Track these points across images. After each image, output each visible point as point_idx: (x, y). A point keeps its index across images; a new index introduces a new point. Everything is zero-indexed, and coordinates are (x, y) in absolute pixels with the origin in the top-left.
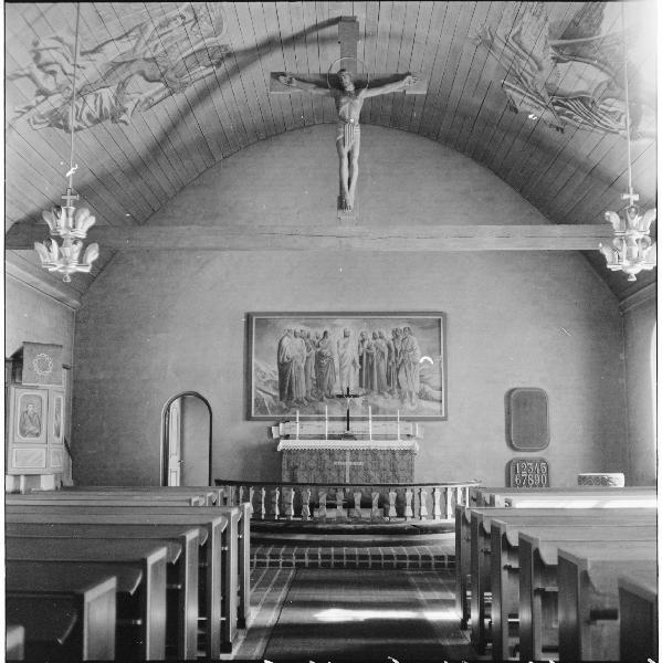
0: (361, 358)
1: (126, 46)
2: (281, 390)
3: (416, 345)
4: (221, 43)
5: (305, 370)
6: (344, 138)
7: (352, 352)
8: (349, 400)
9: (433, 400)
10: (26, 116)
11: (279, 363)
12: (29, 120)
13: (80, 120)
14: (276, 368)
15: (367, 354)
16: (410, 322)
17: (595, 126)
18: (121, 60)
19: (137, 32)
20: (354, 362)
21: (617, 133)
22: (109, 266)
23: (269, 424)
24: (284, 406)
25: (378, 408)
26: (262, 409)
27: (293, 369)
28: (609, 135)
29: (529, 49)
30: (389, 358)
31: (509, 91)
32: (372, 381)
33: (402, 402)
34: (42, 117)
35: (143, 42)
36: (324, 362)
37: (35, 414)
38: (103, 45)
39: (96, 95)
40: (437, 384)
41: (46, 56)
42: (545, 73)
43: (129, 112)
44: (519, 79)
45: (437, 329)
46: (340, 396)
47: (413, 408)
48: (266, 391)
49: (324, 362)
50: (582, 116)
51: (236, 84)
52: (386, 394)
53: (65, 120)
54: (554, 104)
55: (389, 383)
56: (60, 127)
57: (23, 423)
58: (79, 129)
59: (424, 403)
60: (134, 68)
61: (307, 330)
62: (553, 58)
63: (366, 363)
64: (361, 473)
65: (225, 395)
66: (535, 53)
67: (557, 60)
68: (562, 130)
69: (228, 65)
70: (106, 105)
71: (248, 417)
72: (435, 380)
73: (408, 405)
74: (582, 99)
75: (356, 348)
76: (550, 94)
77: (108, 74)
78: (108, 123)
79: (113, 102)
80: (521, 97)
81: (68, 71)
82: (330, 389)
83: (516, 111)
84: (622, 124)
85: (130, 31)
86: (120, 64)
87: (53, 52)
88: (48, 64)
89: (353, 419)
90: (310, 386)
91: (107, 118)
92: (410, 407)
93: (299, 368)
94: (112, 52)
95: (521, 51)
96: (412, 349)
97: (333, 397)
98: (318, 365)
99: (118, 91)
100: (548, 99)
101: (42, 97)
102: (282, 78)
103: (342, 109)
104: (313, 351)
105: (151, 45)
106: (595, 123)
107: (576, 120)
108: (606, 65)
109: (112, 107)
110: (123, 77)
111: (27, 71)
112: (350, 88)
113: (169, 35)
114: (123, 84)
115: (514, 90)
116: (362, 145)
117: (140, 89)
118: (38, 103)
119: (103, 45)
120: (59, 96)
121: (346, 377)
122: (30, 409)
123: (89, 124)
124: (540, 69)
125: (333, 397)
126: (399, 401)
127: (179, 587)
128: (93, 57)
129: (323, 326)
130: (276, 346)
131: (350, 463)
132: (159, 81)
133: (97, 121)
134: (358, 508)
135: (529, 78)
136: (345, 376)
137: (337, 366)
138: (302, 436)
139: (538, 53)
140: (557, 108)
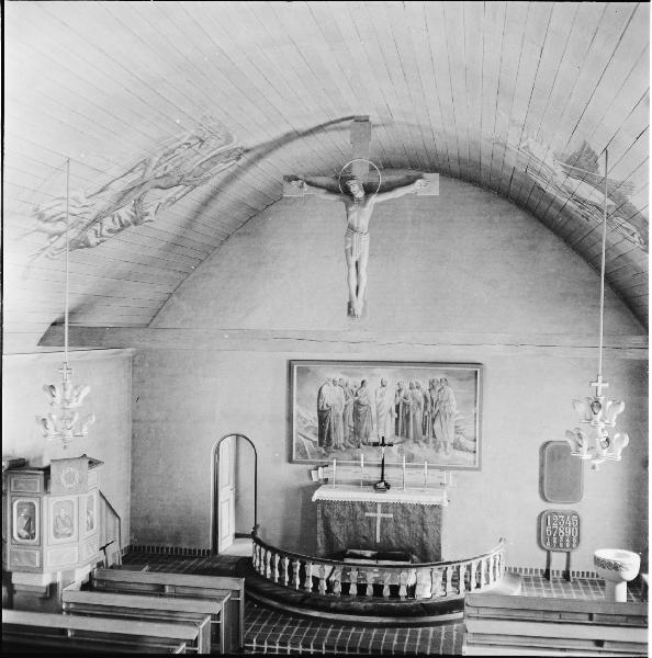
0: (397, 407)
2: (321, 436)
3: (452, 396)
5: (344, 417)
6: (352, 248)
7: (389, 402)
8: (383, 449)
9: (467, 450)
11: (319, 410)
15: (404, 404)
16: (447, 373)
22: (161, 312)
23: (310, 467)
25: (413, 455)
26: (304, 454)
27: (332, 416)
30: (425, 408)
33: (437, 451)
36: (362, 410)
37: (67, 517)
40: (471, 435)
41: (49, 214)
45: (474, 381)
46: (376, 444)
47: (448, 457)
48: (307, 435)
49: (362, 410)
51: (253, 171)
52: (422, 443)
55: (424, 433)
57: (56, 526)
59: (458, 454)
60: (146, 187)
61: (345, 378)
63: (402, 413)
64: (391, 526)
65: (269, 441)
69: (248, 156)
71: (290, 460)
72: (469, 431)
73: (442, 454)
82: (367, 436)
89: (388, 465)
90: (348, 433)
91: (129, 225)
92: (444, 457)
93: (338, 416)
97: (369, 444)
98: (356, 414)
103: (350, 218)
104: (351, 400)
110: (137, 196)
112: (360, 194)
116: (371, 255)
121: (382, 426)
122: (62, 513)
125: (369, 444)
126: (433, 451)
129: (361, 375)
131: (382, 515)
136: (383, 425)
137: (374, 414)
138: (341, 487)
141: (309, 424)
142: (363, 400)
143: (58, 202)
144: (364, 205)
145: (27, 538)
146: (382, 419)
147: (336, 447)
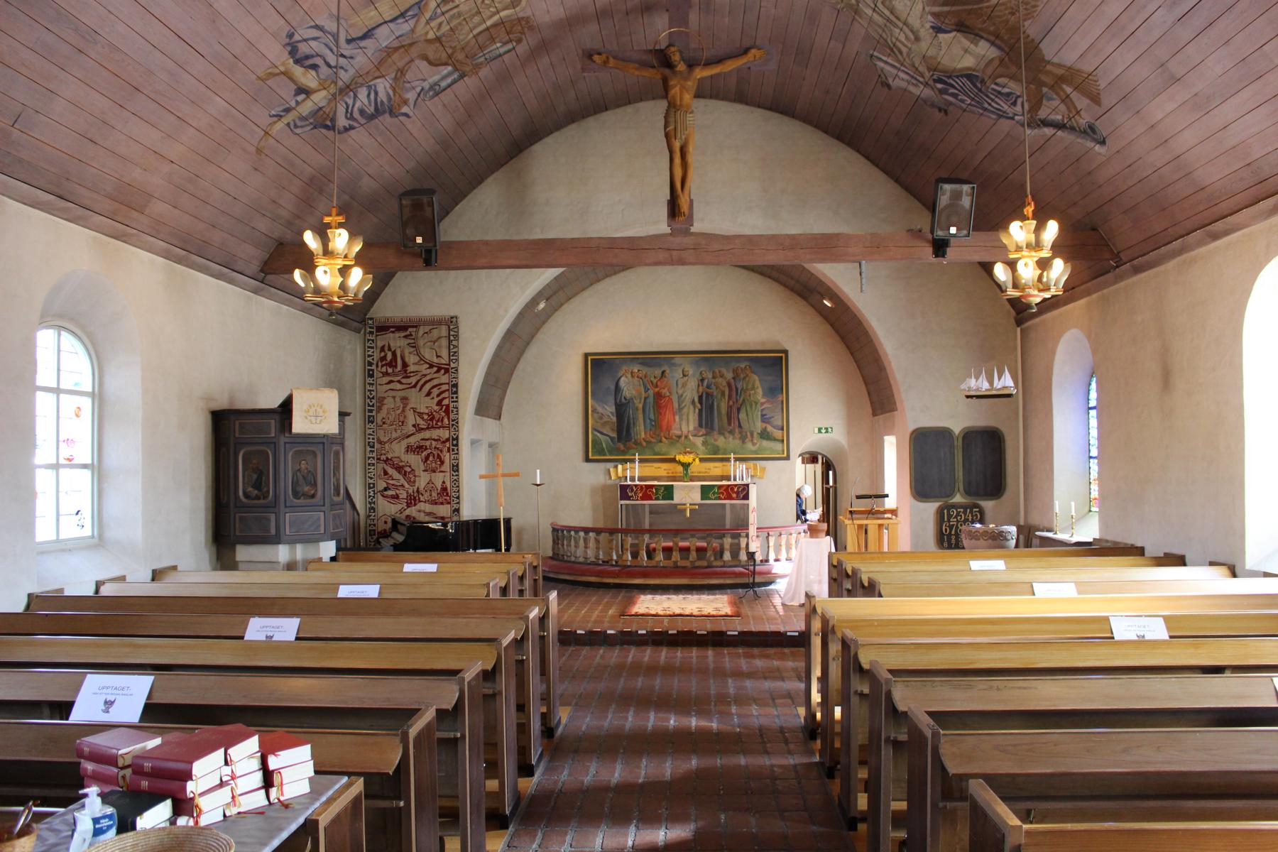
0: (700, 398)
1: (404, 27)
2: (619, 431)
4: (521, 15)
9: (775, 440)
10: (285, 120)
12: (288, 125)
13: (352, 118)
14: (613, 409)
17: (986, 109)
18: (396, 44)
19: (415, 10)
20: (693, 402)
21: (1013, 119)
24: (622, 447)
28: (1002, 120)
29: (903, 17)
31: (881, 64)
32: (712, 420)
33: (743, 442)
34: (302, 118)
35: (423, 21)
38: (374, 29)
39: (369, 87)
41: (304, 49)
42: (924, 45)
43: (412, 102)
44: (892, 50)
47: (753, 448)
50: (969, 96)
53: (333, 120)
54: (935, 81)
55: (729, 424)
56: (327, 127)
58: (352, 128)
59: (765, 443)
60: (414, 52)
62: (932, 27)
66: (910, 20)
67: (938, 30)
68: (946, 112)
70: (382, 96)
71: (587, 460)
73: (749, 445)
74: (969, 77)
75: (695, 388)
76: (929, 69)
77: (382, 62)
78: (386, 118)
79: (391, 93)
80: (895, 71)
81: (333, 63)
83: (889, 86)
84: (1018, 108)
85: (407, 11)
86: (396, 49)
87: (313, 44)
88: (307, 57)
91: (384, 112)
94: (385, 37)
95: (892, 18)
96: (753, 388)
99: (396, 79)
100: (927, 75)
101: (303, 96)
102: (596, 58)
104: (651, 392)
105: (433, 24)
106: (986, 105)
107: (963, 101)
108: (997, 37)
109: (390, 99)
110: (400, 64)
111: (282, 69)
112: (681, 67)
113: (455, 11)
114: (402, 72)
115: (886, 63)
117: (424, 75)
118: (298, 103)
119: (374, 29)
120: (324, 93)
123: (363, 121)
124: (917, 39)
127: (402, 804)
128: (363, 44)
130: (613, 387)
132: (446, 64)
133: (371, 117)
134: (693, 548)
135: (904, 50)
137: (676, 405)
139: (915, 21)
140: (940, 86)
141: (605, 419)
142: (665, 392)
143: (316, 33)
144: (686, 79)
145: (258, 498)
146: (685, 410)
147: (636, 443)
